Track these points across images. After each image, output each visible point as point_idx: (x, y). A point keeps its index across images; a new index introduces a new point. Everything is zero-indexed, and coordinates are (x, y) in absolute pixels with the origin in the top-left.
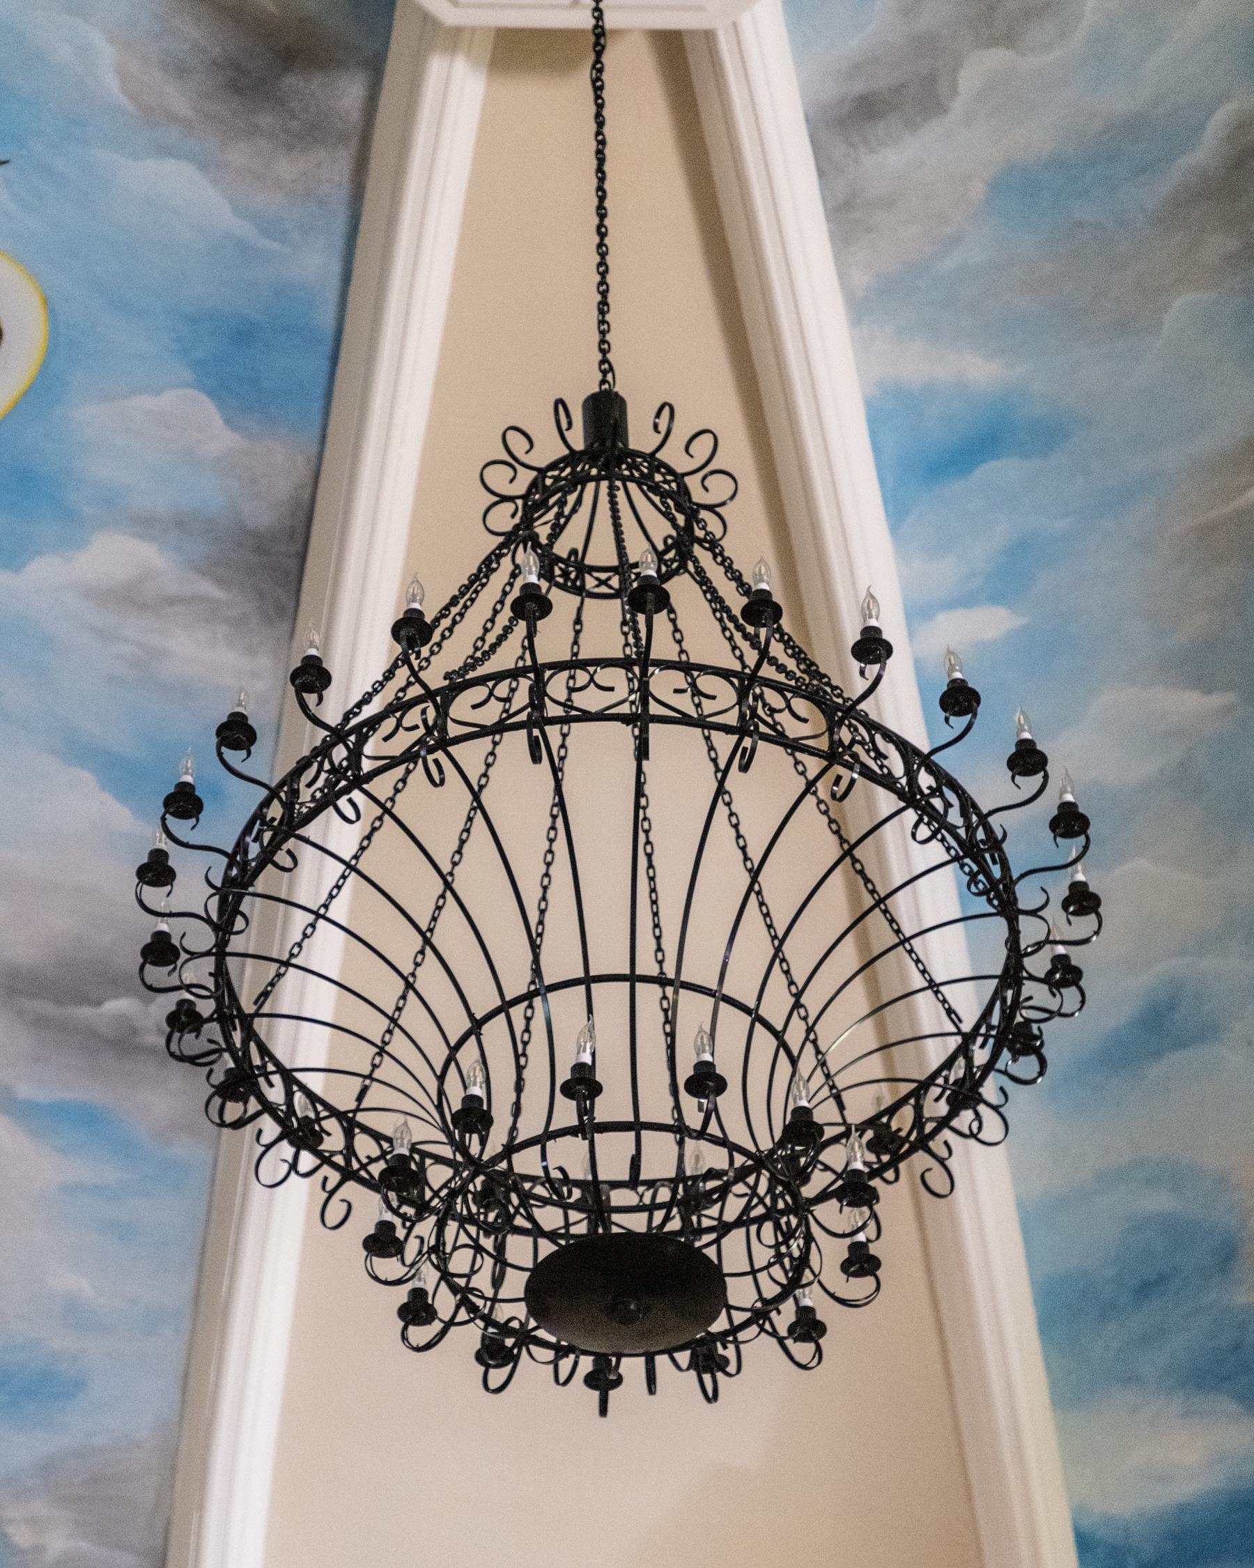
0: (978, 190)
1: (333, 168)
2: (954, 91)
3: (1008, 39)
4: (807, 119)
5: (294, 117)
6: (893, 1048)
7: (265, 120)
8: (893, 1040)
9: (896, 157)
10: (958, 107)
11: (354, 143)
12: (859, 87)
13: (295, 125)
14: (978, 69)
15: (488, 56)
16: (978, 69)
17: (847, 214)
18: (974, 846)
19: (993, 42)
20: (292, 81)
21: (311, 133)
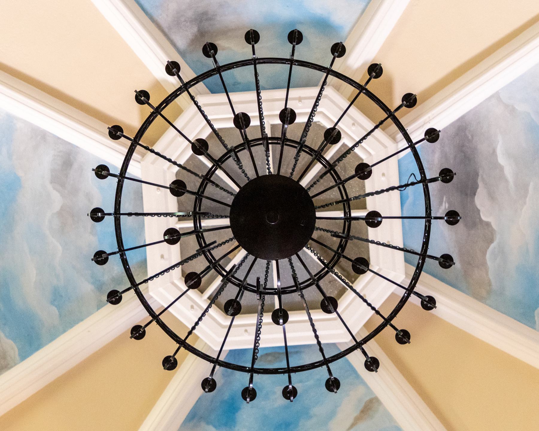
0: (20, 173)
1: (164, 19)
2: (54, 189)
3: (60, 214)
4: (77, 147)
5: (185, 21)
6: (147, 247)
7: (190, 14)
8: (147, 243)
9: (46, 161)
10: (50, 187)
11: (166, 30)
12: (75, 166)
13: (183, 19)
14: (57, 200)
15: (162, 84)
16: (57, 200)
17: (41, 137)
18: (363, 169)
19: (62, 209)
20: (195, 29)
21: (177, 22)
